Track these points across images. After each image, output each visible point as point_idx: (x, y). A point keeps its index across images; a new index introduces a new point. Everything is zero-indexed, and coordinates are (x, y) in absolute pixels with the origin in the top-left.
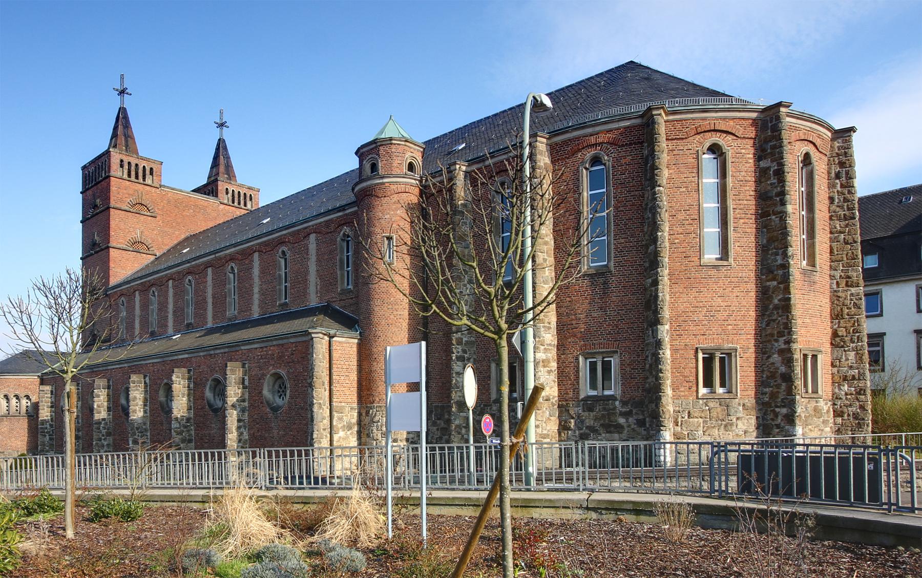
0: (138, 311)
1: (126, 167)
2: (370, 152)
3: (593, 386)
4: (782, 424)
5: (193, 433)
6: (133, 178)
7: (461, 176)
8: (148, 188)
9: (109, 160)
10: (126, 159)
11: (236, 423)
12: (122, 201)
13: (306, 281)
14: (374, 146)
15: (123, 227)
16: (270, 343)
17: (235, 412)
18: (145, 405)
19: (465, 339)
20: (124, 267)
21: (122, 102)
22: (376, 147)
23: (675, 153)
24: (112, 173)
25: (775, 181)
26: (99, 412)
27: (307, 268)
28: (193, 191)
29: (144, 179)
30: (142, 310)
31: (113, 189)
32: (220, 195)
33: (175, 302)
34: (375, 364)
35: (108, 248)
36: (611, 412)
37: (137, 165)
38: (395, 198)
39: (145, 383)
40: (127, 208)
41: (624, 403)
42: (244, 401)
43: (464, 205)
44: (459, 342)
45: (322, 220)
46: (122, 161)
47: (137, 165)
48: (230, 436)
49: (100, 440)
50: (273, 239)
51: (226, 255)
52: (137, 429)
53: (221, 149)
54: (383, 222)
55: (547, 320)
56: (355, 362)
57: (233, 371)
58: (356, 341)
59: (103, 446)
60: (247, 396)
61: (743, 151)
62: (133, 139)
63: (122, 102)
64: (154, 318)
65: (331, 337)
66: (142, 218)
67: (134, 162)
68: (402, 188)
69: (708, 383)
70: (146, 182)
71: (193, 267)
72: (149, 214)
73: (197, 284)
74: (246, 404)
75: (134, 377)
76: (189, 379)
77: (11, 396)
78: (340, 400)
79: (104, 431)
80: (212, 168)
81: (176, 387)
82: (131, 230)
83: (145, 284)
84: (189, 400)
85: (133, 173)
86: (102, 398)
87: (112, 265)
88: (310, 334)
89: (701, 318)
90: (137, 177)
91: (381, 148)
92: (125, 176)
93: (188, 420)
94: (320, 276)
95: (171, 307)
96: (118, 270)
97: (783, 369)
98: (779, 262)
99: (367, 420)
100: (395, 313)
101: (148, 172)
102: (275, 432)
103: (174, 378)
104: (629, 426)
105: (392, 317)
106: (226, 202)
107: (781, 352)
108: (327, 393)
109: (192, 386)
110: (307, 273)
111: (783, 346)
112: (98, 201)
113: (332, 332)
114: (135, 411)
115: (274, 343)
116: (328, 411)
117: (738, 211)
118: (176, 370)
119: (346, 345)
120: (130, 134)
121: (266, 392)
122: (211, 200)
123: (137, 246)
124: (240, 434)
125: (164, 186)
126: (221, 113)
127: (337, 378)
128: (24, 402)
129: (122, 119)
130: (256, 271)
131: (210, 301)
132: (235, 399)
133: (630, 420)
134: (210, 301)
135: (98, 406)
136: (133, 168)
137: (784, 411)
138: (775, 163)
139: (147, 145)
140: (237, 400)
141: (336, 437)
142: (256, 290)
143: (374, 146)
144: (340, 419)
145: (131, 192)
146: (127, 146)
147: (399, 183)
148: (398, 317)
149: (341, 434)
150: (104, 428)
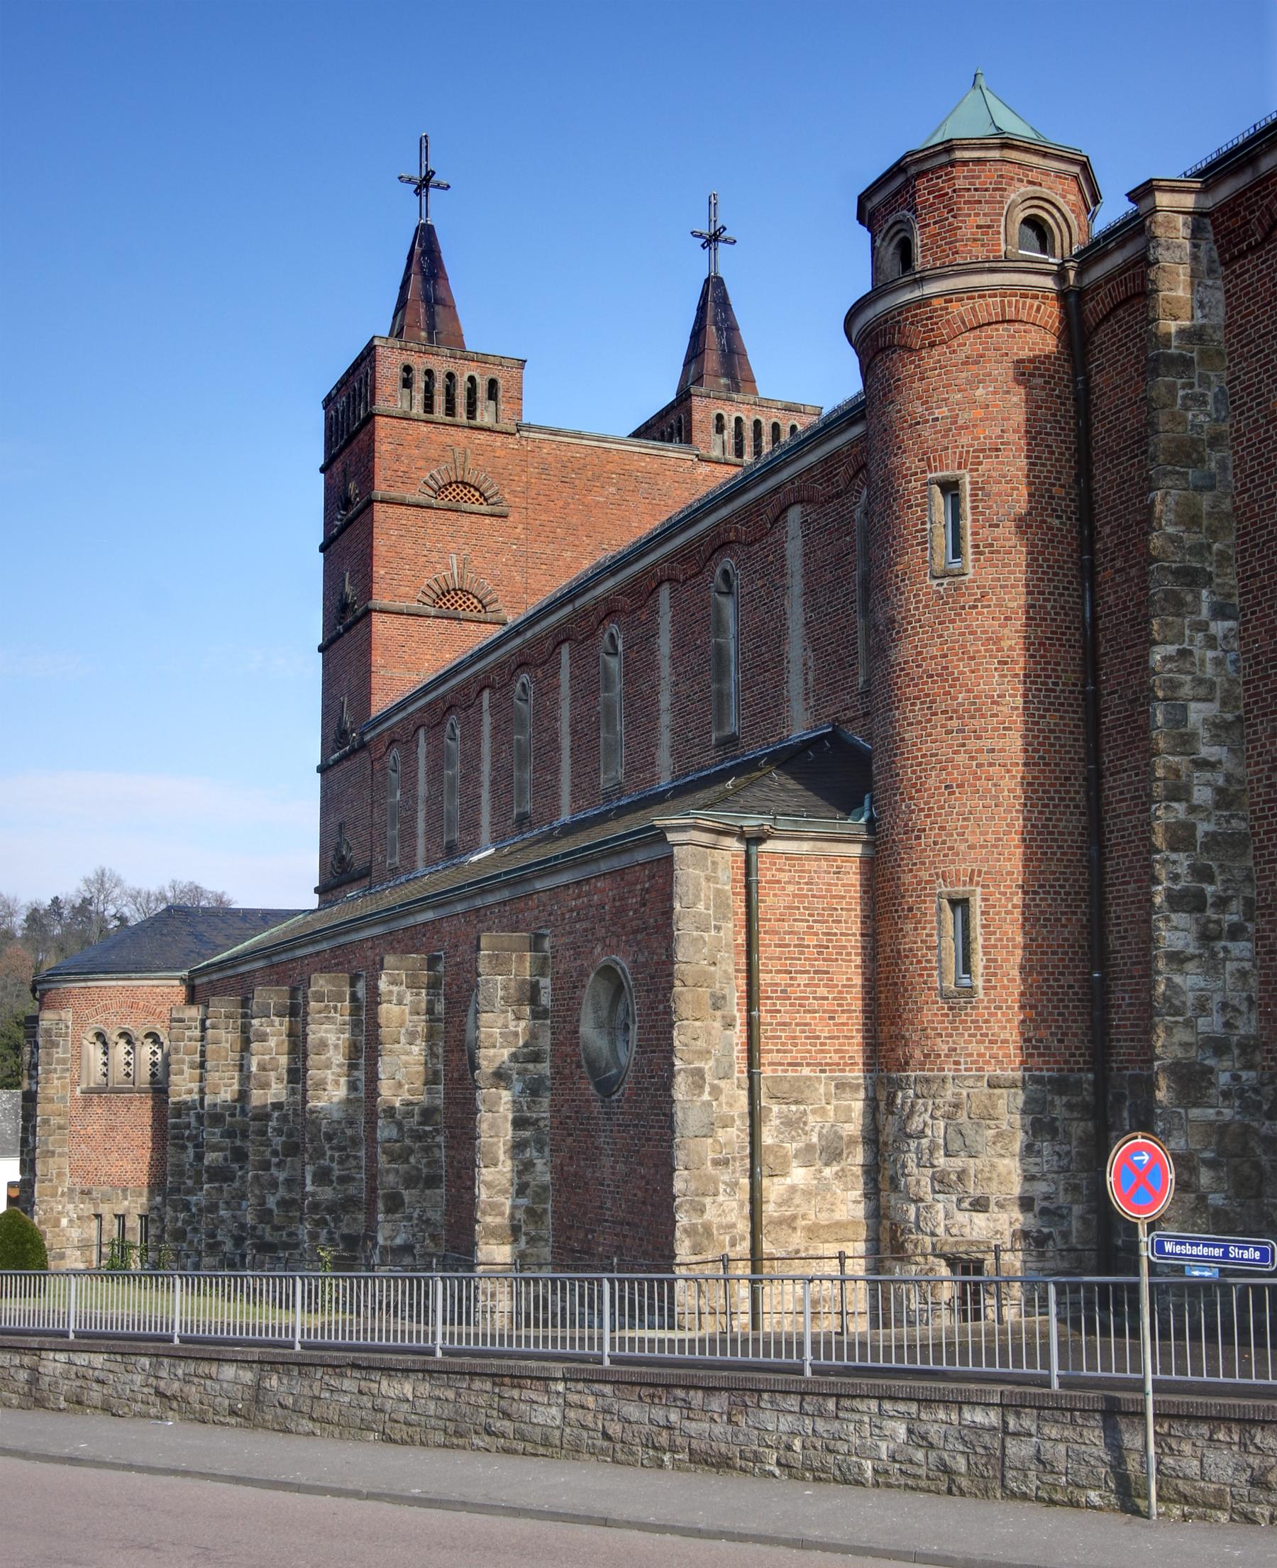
0: (422, 789)
1: (420, 383)
2: (890, 205)
5: (441, 1155)
6: (439, 413)
7: (1180, 229)
8: (483, 436)
9: (373, 368)
10: (420, 364)
11: (508, 1132)
12: (406, 479)
13: (780, 659)
14: (900, 180)
15: (409, 552)
16: (593, 869)
17: (506, 1096)
18: (352, 1066)
19: (1203, 828)
20: (409, 659)
21: (713, 262)
22: (908, 183)
24: (380, 405)
26: (265, 1085)
27: (782, 618)
28: (637, 434)
29: (471, 413)
30: (430, 783)
31: (383, 448)
32: (697, 435)
33: (496, 754)
34: (909, 927)
35: (368, 612)
37: (450, 376)
38: (969, 344)
39: (354, 998)
40: (422, 499)
42: (536, 1058)
43: (1192, 335)
44: (1181, 838)
45: (812, 458)
46: (407, 369)
47: (450, 376)
48: (486, 1173)
49: (266, 1166)
50: (701, 537)
51: (598, 601)
52: (329, 1137)
53: (714, 299)
54: (926, 432)
56: (855, 927)
57: (499, 963)
58: (857, 850)
59: (274, 1185)
60: (545, 1043)
62: (451, 307)
63: (713, 262)
64: (452, 805)
65: (753, 840)
66: (466, 521)
67: (441, 367)
68: (988, 308)
70: (478, 421)
71: (529, 645)
72: (485, 508)
73: (541, 694)
74: (545, 1068)
75: (321, 983)
76: (433, 986)
77: (112, 1036)
78: (795, 1055)
79: (278, 1142)
80: (687, 364)
81: (388, 1011)
82: (435, 556)
83: (446, 702)
84: (431, 1053)
85: (439, 400)
86: (272, 1042)
87: (377, 659)
88: (663, 831)
90: (450, 410)
91: (922, 184)
92: (418, 410)
93: (428, 1114)
94: (814, 642)
95: (486, 767)
96: (397, 673)
99: (890, 1128)
100: (972, 744)
101: (482, 392)
102: (607, 1162)
103: (383, 985)
105: (962, 758)
106: (716, 453)
108: (738, 1035)
109: (440, 1008)
110: (780, 635)
112: (352, 486)
113: (751, 823)
114: (321, 1085)
115: (604, 866)
116: (743, 1096)
118: (389, 960)
119: (815, 868)
120: (441, 293)
121: (588, 1030)
122: (673, 452)
123: (450, 601)
124: (524, 1168)
125: (530, 427)
126: (712, 204)
127: (782, 979)
128: (146, 1051)
129: (426, 257)
130: (664, 643)
131: (566, 742)
132: (506, 1053)
134: (566, 742)
135: (262, 1068)
136: (439, 387)
139: (485, 318)
140: (514, 1057)
141: (773, 1189)
142: (665, 700)
143: (900, 180)
144: (793, 1124)
145: (433, 453)
146: (431, 327)
147: (980, 292)
148: (983, 758)
149: (799, 1175)
150: (279, 1132)
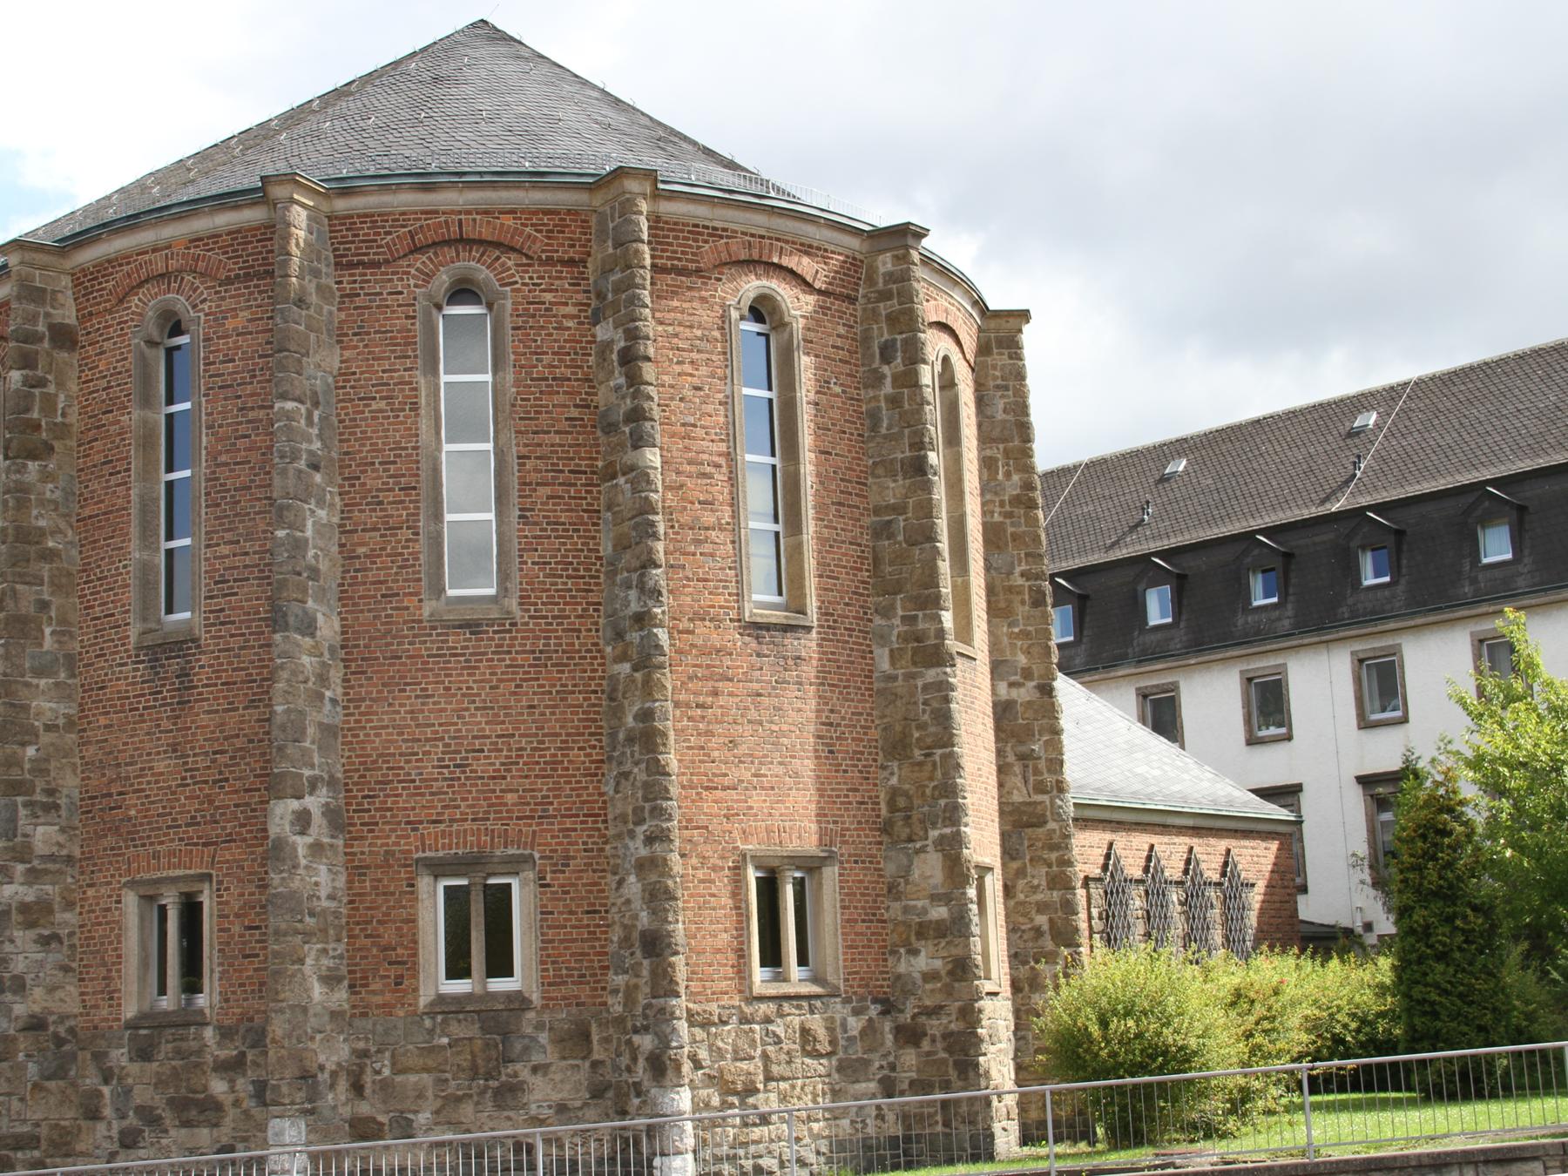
3: (458, 968)
4: (646, 1083)
23: (358, 301)
25: (622, 380)
36: (191, 1059)
41: (225, 1033)
55: (40, 784)
61: (548, 297)
69: (772, 956)
89: (429, 770)
97: (644, 919)
98: (634, 607)
104: (237, 1103)
107: (642, 866)
111: (644, 852)
117: (529, 464)
133: (241, 1083)
137: (646, 1042)
138: (620, 330)
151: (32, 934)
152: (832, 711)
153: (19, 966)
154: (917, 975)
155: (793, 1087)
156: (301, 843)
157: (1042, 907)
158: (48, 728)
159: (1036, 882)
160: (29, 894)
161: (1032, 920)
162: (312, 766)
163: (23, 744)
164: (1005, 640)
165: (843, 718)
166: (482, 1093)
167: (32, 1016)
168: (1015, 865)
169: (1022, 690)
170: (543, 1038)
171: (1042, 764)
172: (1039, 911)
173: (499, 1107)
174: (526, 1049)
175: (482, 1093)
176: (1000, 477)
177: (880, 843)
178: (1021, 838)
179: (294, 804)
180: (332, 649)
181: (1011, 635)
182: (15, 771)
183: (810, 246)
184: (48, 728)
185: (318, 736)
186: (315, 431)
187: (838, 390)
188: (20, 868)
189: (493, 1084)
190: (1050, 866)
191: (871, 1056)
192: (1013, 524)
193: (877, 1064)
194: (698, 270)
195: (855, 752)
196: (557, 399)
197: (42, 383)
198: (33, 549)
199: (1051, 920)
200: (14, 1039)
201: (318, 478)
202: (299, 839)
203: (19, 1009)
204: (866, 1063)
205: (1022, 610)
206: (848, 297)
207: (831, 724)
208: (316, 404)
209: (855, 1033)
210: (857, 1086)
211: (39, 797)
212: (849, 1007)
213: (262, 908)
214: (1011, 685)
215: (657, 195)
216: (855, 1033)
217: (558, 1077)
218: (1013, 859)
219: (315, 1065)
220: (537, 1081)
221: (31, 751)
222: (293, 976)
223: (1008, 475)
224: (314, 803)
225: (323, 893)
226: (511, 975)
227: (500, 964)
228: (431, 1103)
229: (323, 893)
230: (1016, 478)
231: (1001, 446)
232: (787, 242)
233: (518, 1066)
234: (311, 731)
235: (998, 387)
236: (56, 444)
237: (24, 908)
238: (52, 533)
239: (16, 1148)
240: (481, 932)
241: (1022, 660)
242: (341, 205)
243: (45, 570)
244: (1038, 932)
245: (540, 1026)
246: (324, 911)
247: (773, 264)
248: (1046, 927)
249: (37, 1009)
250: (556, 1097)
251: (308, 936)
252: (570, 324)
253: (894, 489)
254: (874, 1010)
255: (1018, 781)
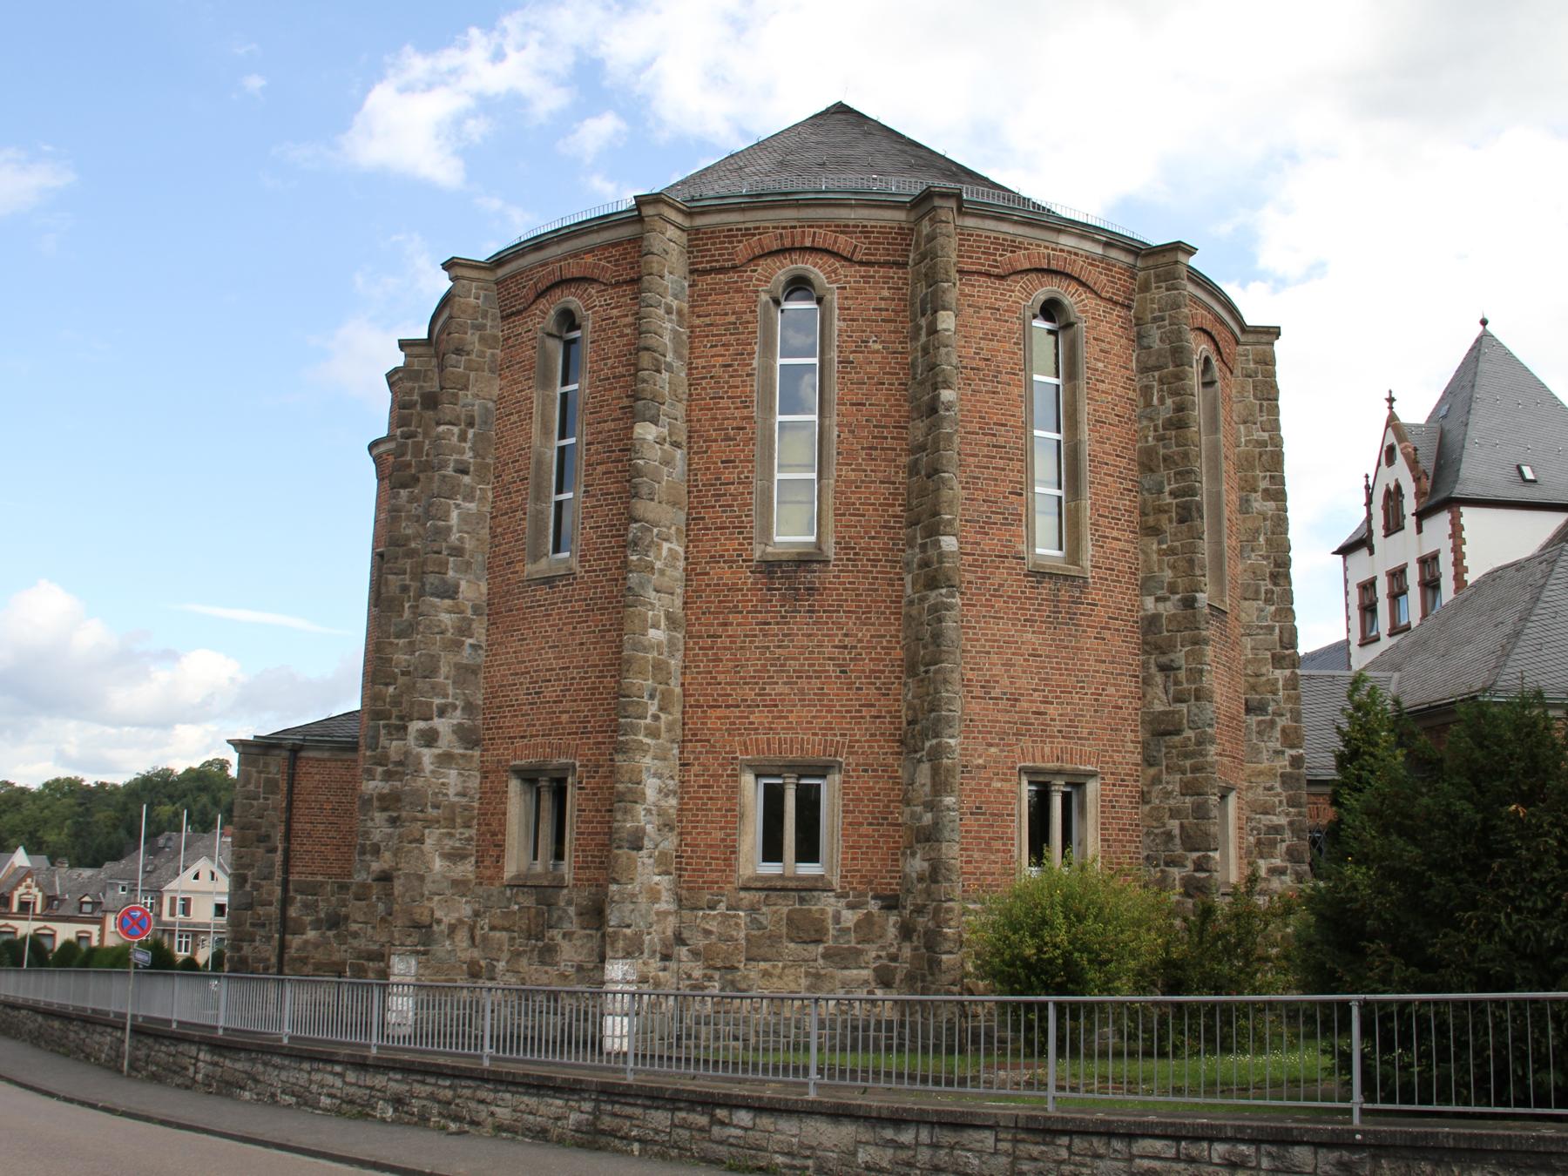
3: (772, 851)
55: (395, 712)
61: (615, 312)
117: (593, 448)
151: (385, 815)
152: (846, 635)
153: (376, 836)
154: (914, 875)
155: (774, 967)
156: (427, 756)
157: (1174, 813)
158: (403, 673)
159: (1170, 787)
160: (385, 787)
161: (1164, 825)
162: (446, 696)
163: (387, 685)
164: (1155, 557)
165: (860, 641)
166: (532, 951)
167: (383, 871)
168: (1152, 771)
169: (1169, 604)
170: (572, 910)
171: (1182, 675)
172: (1171, 817)
173: (543, 963)
174: (560, 918)
175: (532, 951)
176: (1155, 401)
177: (900, 753)
178: (1158, 744)
179: (421, 725)
180: (476, 609)
181: (1161, 552)
182: (380, 703)
183: (847, 226)
184: (403, 673)
185: (453, 673)
186: (467, 445)
187: (878, 346)
188: (380, 769)
189: (540, 944)
190: (1184, 773)
191: (866, 946)
192: (1165, 447)
193: (874, 954)
194: (734, 268)
195: (872, 671)
196: (615, 393)
197: (412, 435)
198: (401, 550)
199: (1182, 826)
200: (370, 887)
201: (466, 479)
202: (425, 751)
203: (375, 866)
204: (858, 953)
205: (1169, 528)
206: (896, 264)
207: (845, 647)
208: (471, 424)
209: (850, 924)
210: (847, 972)
211: (394, 721)
212: (843, 902)
213: (615, 798)
214: (1158, 600)
215: (961, 211)
216: (850, 924)
217: (579, 943)
218: (1151, 765)
219: (223, 920)
220: (565, 945)
221: (391, 689)
222: (409, 851)
223: (1162, 400)
224: (443, 725)
225: (451, 792)
226: (765, 860)
227: (808, 850)
228: (505, 956)
229: (451, 792)
230: (1169, 402)
231: (1156, 374)
232: (820, 227)
233: (555, 932)
234: (444, 670)
235: (1155, 320)
236: (422, 476)
237: (382, 797)
238: (415, 538)
239: (369, 959)
240: (795, 823)
241: (1168, 574)
242: (501, 272)
243: (408, 564)
244: (1169, 836)
245: (569, 903)
246: (453, 806)
247: (806, 249)
248: (1177, 832)
249: (386, 866)
250: (577, 958)
251: (429, 823)
252: (628, 331)
253: (918, 430)
254: (873, 906)
255: (1159, 691)
